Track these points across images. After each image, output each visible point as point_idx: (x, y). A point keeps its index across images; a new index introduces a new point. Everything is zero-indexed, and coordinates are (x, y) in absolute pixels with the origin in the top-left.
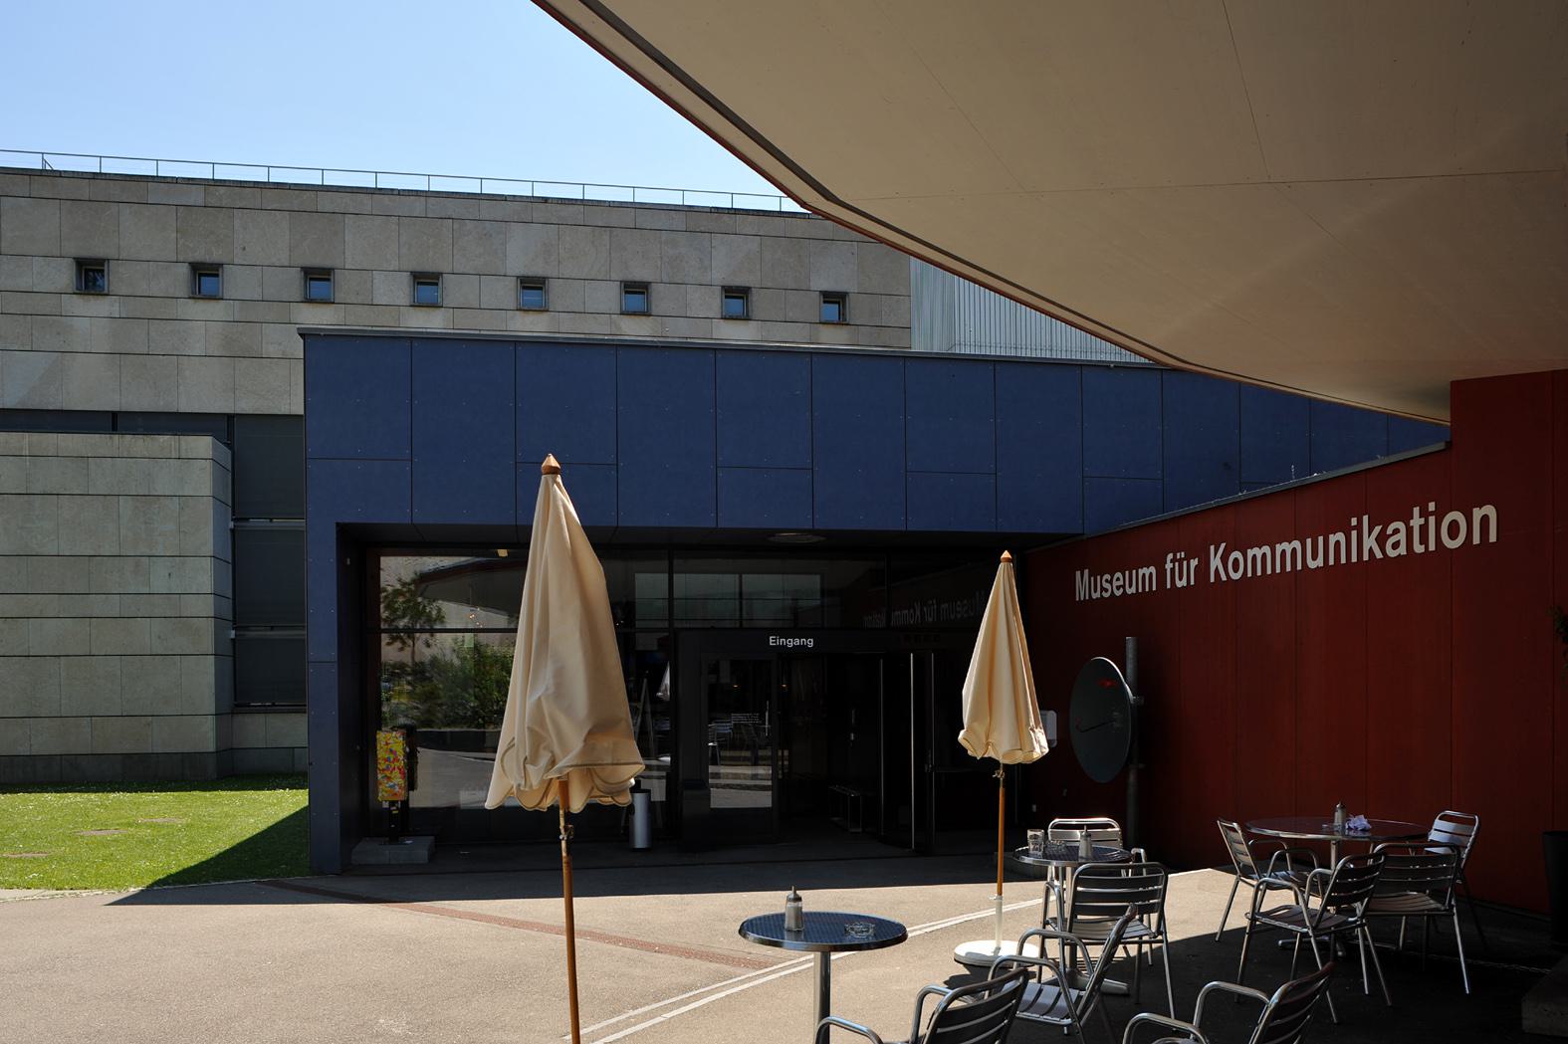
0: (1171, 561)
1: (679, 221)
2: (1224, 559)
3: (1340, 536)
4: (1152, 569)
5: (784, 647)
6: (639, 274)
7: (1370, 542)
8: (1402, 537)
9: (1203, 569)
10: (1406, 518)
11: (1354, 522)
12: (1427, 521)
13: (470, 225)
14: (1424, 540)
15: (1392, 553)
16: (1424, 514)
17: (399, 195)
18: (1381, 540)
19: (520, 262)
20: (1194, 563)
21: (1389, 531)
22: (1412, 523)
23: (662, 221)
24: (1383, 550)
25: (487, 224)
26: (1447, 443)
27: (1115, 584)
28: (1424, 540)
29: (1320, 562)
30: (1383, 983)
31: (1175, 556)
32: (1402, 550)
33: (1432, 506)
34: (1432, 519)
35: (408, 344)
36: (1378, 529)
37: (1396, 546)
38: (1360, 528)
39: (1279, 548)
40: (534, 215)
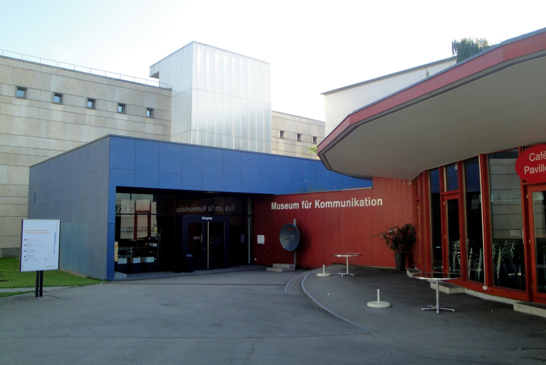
0: (304, 202)
1: (106, 81)
2: (319, 203)
3: (349, 201)
4: (298, 204)
5: (206, 220)
6: (93, 97)
7: (356, 203)
8: (363, 203)
9: (313, 205)
10: (364, 199)
11: (352, 199)
12: (368, 200)
13: (38, 73)
14: (368, 203)
15: (361, 205)
16: (368, 199)
17: (14, 60)
18: (359, 203)
19: (55, 87)
20: (310, 203)
21: (360, 201)
22: (365, 200)
23: (100, 80)
24: (359, 204)
25: (44, 74)
26: (148, 110)
27: (285, 206)
28: (368, 203)
29: (344, 206)
30: (523, 232)
31: (305, 201)
32: (363, 205)
33: (369, 198)
34: (369, 200)
35: (135, 140)
36: (358, 201)
37: (362, 204)
38: (354, 200)
39: (334, 202)
40: (60, 73)
